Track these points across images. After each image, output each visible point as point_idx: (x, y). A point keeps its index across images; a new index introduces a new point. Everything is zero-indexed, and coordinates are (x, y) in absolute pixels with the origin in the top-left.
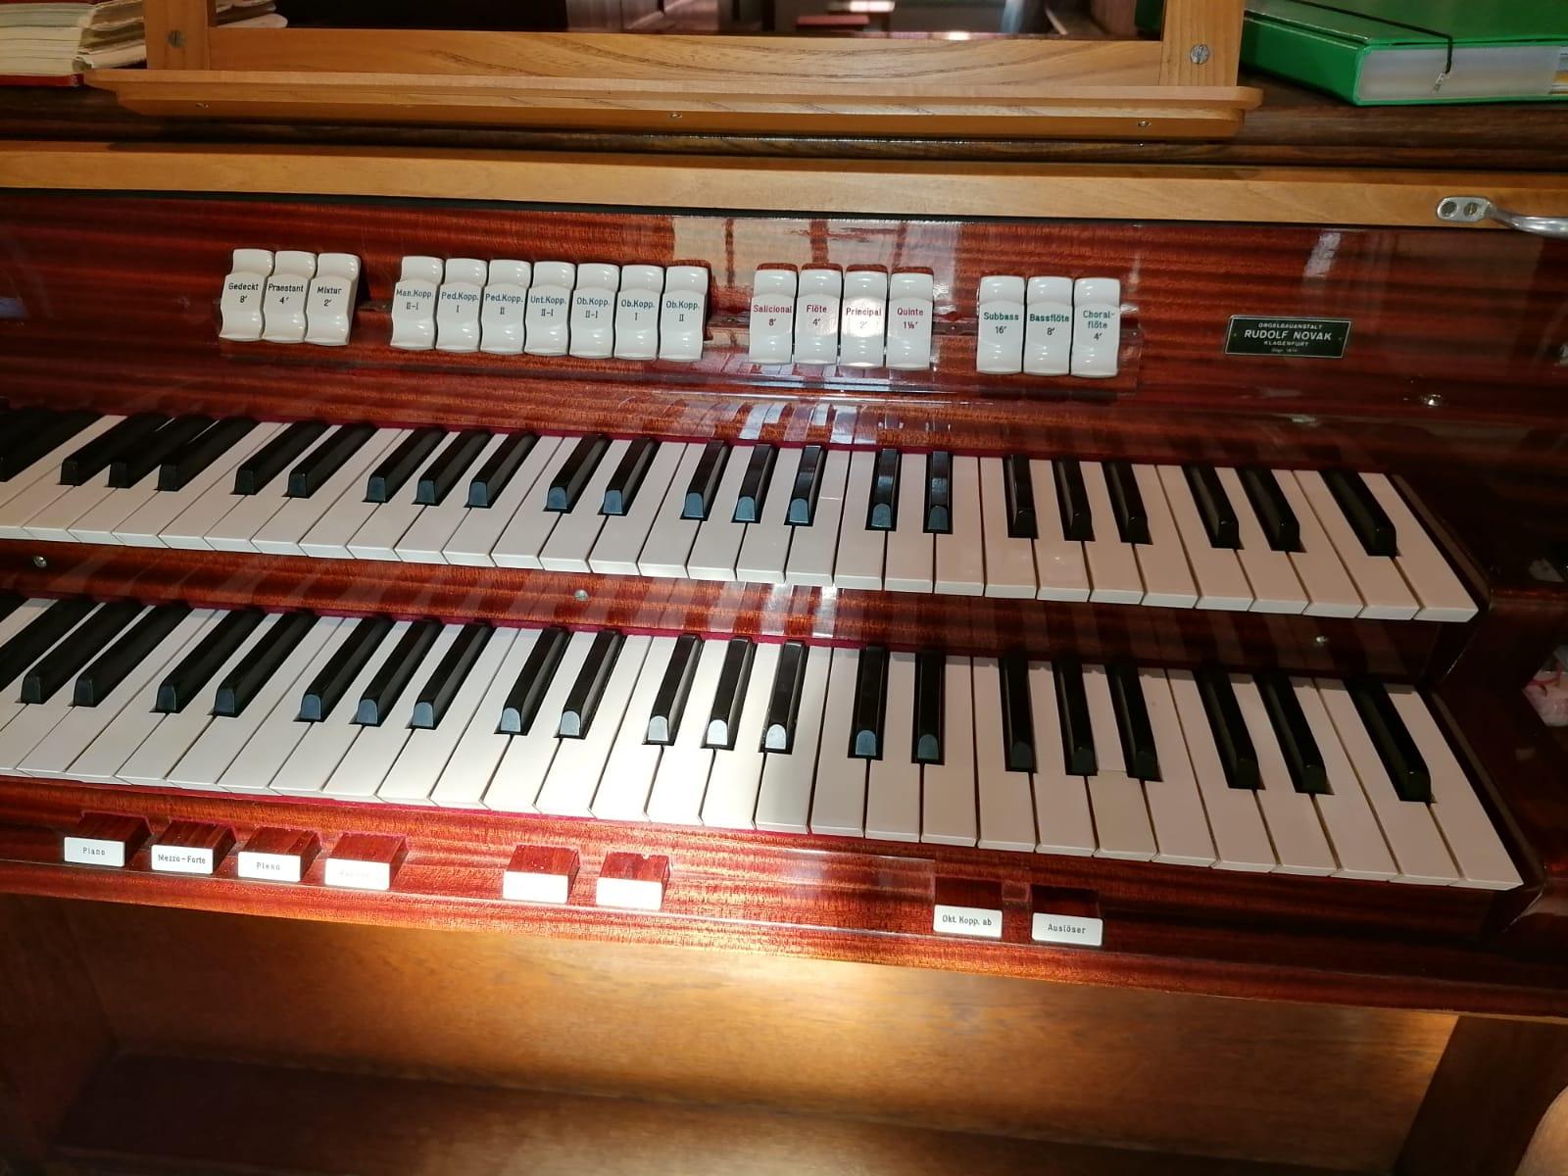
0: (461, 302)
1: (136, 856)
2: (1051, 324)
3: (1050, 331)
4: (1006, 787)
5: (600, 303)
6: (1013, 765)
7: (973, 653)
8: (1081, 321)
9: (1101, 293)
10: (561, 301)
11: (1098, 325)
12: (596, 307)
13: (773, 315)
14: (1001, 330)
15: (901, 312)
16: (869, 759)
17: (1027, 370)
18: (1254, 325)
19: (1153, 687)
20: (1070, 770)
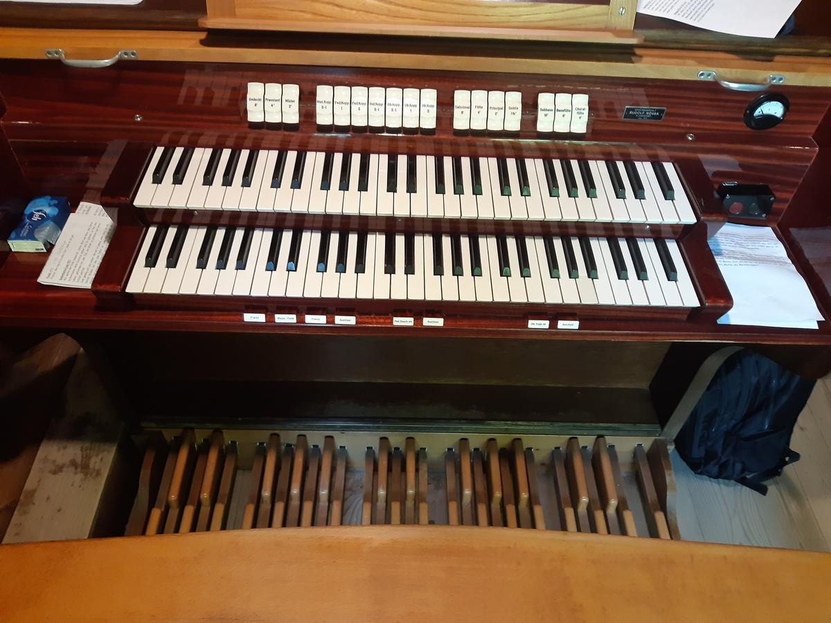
0: (343, 105)
1: (553, 325)
2: (564, 113)
3: (564, 116)
4: (551, 283)
5: (380, 104)
6: (456, 273)
7: (423, 233)
8: (575, 112)
9: (582, 100)
10: (382, 105)
11: (581, 113)
12: (326, 104)
13: (463, 110)
14: (546, 115)
15: (510, 108)
16: (323, 272)
17: (505, 129)
18: (633, 110)
19: (594, 243)
20: (386, 272)
